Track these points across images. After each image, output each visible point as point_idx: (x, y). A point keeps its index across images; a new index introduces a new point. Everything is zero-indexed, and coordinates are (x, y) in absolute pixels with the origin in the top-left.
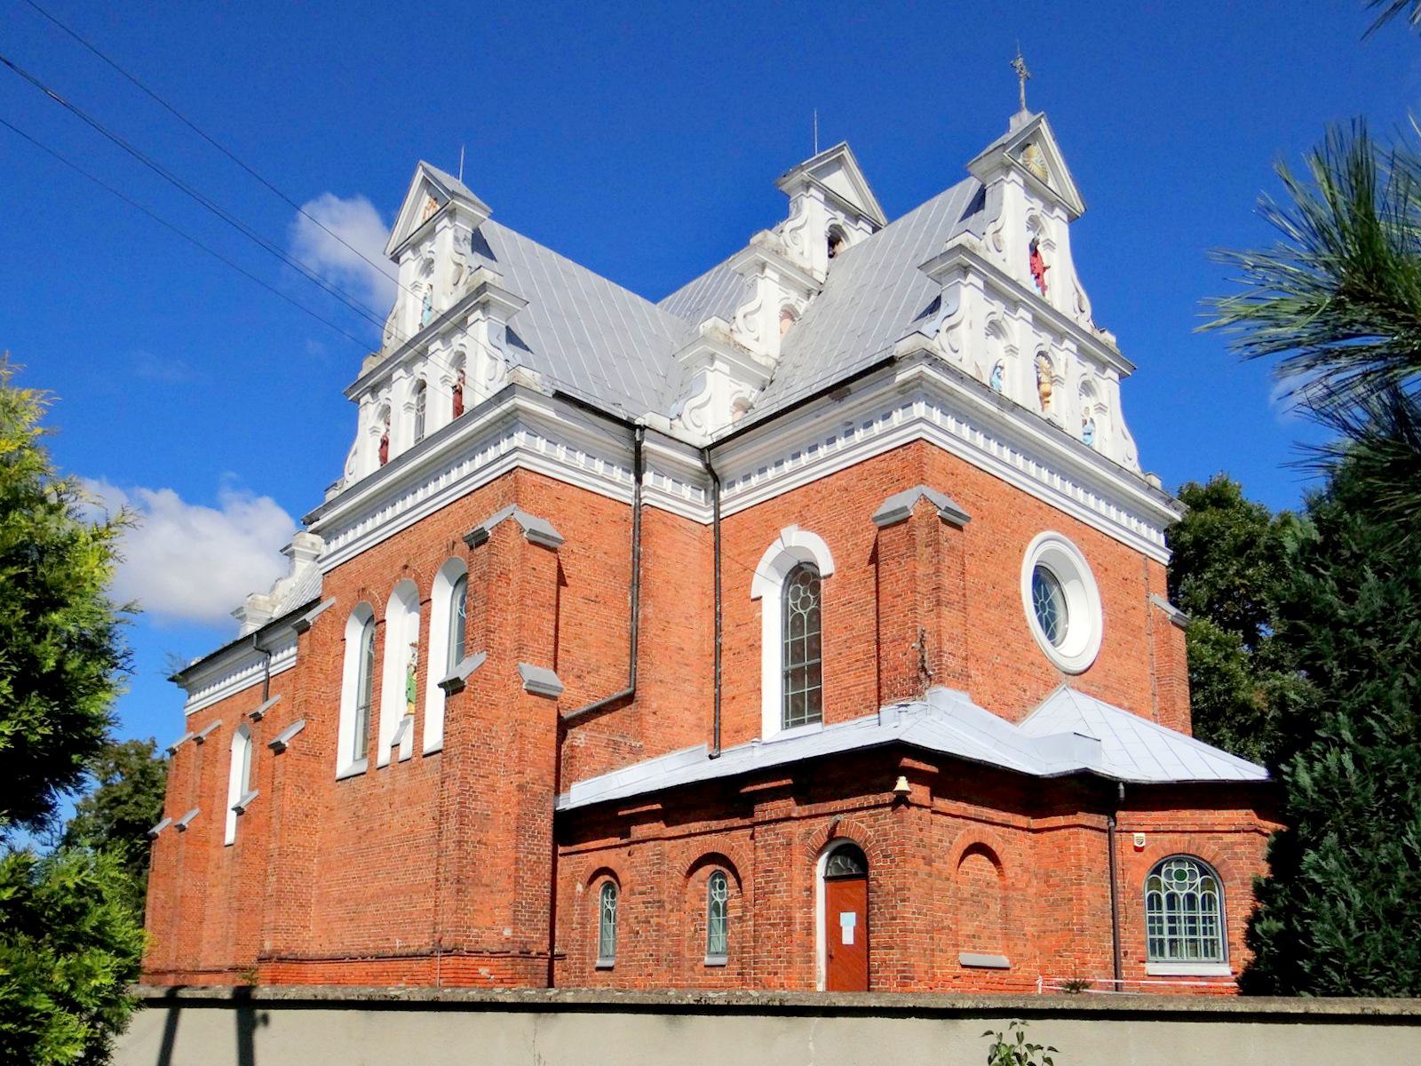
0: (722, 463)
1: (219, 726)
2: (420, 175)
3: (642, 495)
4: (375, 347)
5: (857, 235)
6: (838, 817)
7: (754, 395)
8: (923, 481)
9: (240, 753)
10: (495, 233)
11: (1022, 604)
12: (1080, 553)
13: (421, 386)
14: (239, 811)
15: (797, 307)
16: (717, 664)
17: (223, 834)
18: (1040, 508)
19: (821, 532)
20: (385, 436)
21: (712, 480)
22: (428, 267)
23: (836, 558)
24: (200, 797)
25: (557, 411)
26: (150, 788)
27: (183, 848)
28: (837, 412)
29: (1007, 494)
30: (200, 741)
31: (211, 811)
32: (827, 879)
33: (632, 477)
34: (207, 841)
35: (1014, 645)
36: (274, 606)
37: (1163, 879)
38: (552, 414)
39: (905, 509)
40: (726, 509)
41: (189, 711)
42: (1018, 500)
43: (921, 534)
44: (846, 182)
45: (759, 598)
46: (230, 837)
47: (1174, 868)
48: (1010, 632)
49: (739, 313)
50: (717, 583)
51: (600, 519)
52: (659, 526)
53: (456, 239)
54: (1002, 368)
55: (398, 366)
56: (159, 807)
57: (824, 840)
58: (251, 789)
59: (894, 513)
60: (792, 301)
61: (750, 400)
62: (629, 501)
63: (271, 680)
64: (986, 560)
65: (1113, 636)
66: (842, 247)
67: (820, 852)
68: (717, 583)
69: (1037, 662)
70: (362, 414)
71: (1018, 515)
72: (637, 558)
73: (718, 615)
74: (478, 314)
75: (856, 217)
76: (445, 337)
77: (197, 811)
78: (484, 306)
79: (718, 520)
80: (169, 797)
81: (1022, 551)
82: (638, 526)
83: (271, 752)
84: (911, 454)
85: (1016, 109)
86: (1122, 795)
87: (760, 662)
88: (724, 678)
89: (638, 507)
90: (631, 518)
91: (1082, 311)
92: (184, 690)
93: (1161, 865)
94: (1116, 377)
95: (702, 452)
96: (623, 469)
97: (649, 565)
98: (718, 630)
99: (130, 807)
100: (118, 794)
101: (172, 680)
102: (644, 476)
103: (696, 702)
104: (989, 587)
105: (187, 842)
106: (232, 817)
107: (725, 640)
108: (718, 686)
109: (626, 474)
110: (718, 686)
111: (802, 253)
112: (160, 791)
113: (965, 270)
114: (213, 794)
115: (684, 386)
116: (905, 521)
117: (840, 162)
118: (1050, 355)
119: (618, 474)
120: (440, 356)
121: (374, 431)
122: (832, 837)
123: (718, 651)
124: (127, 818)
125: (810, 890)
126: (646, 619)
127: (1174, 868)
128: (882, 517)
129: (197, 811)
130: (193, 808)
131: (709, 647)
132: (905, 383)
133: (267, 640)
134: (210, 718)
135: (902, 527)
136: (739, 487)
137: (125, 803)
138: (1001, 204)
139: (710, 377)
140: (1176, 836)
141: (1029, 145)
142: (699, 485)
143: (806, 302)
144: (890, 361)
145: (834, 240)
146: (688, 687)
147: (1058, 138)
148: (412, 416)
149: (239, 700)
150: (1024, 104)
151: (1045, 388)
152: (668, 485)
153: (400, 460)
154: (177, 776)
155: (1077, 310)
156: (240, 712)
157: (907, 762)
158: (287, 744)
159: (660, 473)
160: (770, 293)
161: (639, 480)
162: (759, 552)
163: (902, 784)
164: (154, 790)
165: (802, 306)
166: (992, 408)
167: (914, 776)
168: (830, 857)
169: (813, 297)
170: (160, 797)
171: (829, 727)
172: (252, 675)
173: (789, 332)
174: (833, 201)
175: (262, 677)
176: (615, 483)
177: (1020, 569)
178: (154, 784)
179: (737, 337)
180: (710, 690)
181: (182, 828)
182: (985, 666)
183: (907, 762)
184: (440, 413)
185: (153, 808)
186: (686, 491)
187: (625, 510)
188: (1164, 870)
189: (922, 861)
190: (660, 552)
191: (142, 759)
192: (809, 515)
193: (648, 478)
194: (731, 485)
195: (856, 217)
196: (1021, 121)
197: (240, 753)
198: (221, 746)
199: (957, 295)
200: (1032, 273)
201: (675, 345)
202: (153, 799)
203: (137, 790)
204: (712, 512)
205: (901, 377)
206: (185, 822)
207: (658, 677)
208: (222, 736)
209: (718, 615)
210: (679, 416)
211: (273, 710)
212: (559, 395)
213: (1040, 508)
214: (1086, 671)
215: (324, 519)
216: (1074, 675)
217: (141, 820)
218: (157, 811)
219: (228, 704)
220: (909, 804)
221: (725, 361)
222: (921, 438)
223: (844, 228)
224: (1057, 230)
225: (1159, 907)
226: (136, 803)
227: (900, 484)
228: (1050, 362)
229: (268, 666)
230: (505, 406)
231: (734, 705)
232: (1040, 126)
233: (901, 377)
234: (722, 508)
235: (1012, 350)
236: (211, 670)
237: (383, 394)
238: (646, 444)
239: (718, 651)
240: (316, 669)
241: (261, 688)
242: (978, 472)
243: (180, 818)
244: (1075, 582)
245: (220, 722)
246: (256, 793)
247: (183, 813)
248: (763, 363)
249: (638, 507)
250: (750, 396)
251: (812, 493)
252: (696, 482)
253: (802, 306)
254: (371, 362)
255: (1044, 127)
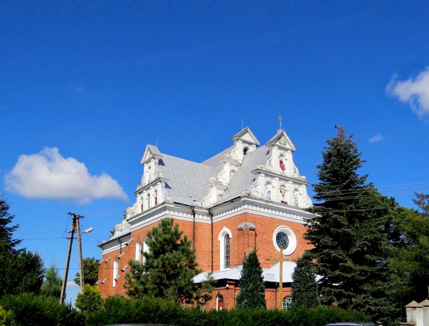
0: (213, 211)
1: (110, 259)
2: (147, 148)
3: (195, 220)
4: (140, 183)
5: (252, 149)
6: (219, 291)
7: (223, 193)
8: (246, 221)
9: (115, 265)
10: (166, 158)
11: (273, 242)
12: (290, 229)
13: (149, 195)
14: (116, 280)
15: (235, 170)
16: (212, 254)
17: (112, 285)
18: (279, 221)
19: (230, 229)
20: (142, 204)
21: (211, 215)
22: (150, 168)
23: (232, 235)
24: (107, 276)
25: (175, 206)
26: (94, 271)
27: (103, 288)
28: (232, 205)
29: (270, 220)
30: (106, 262)
31: (109, 279)
32: (218, 301)
33: (193, 216)
34: (109, 286)
35: (270, 251)
36: (123, 227)
37: (286, 300)
38: (173, 206)
39: (241, 228)
40: (214, 221)
41: (103, 254)
42: (273, 220)
43: (246, 232)
44: (248, 137)
45: (219, 241)
46: (114, 285)
47: (288, 298)
48: (269, 249)
49: (219, 175)
50: (212, 237)
51: (185, 226)
52: (199, 226)
53: (155, 164)
54: (270, 192)
55: (144, 190)
56: (96, 275)
57: (217, 294)
58: (118, 275)
59: (240, 228)
60: (233, 169)
61: (222, 194)
62: (192, 221)
63: (122, 249)
64: (263, 235)
65: (300, 246)
66: (248, 152)
67: (217, 297)
68: (212, 237)
69: (277, 254)
70: (145, 168)
71: (273, 224)
72: (194, 233)
73: (212, 244)
74: (159, 183)
75: (251, 144)
76: (153, 186)
77: (106, 279)
78: (160, 181)
79: (212, 223)
80: (99, 273)
81: (273, 231)
82: (194, 226)
83: (121, 271)
84: (245, 215)
85: (279, 128)
86: (277, 285)
87: (219, 255)
88: (214, 257)
89: (194, 222)
90: (193, 225)
91: (295, 173)
92: (101, 249)
93: (286, 298)
94: (305, 186)
95: (209, 209)
96: (191, 214)
97: (196, 235)
98: (212, 247)
99: (89, 276)
100: (86, 272)
101: (98, 246)
102: (195, 215)
103: (208, 262)
104: (264, 240)
105: (104, 287)
106: (114, 281)
107: (214, 249)
108: (212, 259)
109: (191, 215)
110: (212, 259)
111: (236, 156)
112: (96, 271)
113: (260, 173)
114: (110, 276)
115: (206, 193)
116: (242, 230)
117: (247, 131)
118: (285, 185)
119: (189, 216)
120: (152, 191)
121: (140, 202)
122: (218, 294)
123: (212, 251)
124: (88, 278)
125: (215, 303)
126: (196, 246)
127: (288, 298)
128: (238, 229)
129: (106, 279)
130: (105, 278)
131: (211, 250)
132: (243, 201)
133: (121, 239)
134: (108, 257)
135: (242, 231)
136: (216, 217)
137: (88, 274)
138: (272, 154)
139: (212, 191)
140: (288, 292)
141: (281, 138)
142: (208, 216)
143: (237, 168)
144: (239, 197)
145: (245, 150)
146: (206, 259)
147: (288, 135)
148: (148, 201)
149: (115, 253)
150: (281, 127)
151: (283, 193)
152: (201, 217)
153: (145, 212)
154: (101, 270)
155: (294, 173)
156: (115, 256)
157: (228, 282)
158: (124, 270)
159: (199, 215)
160: (227, 168)
161: (194, 216)
162: (220, 231)
163: (227, 286)
164: (95, 271)
165: (236, 169)
166: (265, 203)
167: (229, 284)
168: (219, 297)
169: (239, 167)
170: (97, 273)
171: (231, 269)
172: (117, 247)
173: (233, 175)
174: (244, 142)
175: (120, 248)
176: (189, 218)
177: (273, 235)
178: (94, 269)
179: (219, 180)
180: (211, 260)
181: (103, 283)
182: (262, 257)
183: (228, 282)
184: (153, 204)
185: (95, 276)
186: (205, 217)
187: (191, 223)
188: (286, 298)
189: (232, 299)
190: (199, 231)
191: (91, 263)
192: (228, 225)
193: (196, 216)
194: (215, 216)
195: (251, 144)
196: (280, 131)
197: (115, 265)
198: (111, 263)
199: (258, 178)
200: (280, 167)
201: (210, 175)
202: (95, 273)
203: (91, 271)
204: (211, 222)
205: (242, 200)
206: (103, 282)
207: (199, 258)
208: (111, 261)
209: (212, 244)
210: (204, 201)
211: (123, 256)
212: (175, 203)
213: (279, 221)
214: (291, 254)
215: (130, 221)
216: (288, 256)
217: (92, 279)
218: (96, 276)
219: (112, 253)
220: (229, 289)
221: (215, 187)
222: (246, 213)
223: (248, 147)
224: (289, 156)
225: (285, 305)
226: (91, 275)
227: (242, 221)
228: (285, 187)
229: (121, 245)
230: (164, 205)
231: (215, 263)
232: (284, 133)
233: (242, 200)
234: (213, 221)
235: (273, 187)
236: (108, 245)
237: (142, 194)
238: (195, 209)
239: (212, 251)
240: (130, 254)
241: (120, 251)
242: (261, 216)
243: (102, 280)
244: (290, 235)
245: (110, 258)
246: (119, 276)
247: (103, 279)
248: (225, 185)
249: (194, 222)
250: (222, 193)
251: (229, 220)
252: (207, 215)
253: (236, 169)
254: (139, 187)
255: (284, 133)
